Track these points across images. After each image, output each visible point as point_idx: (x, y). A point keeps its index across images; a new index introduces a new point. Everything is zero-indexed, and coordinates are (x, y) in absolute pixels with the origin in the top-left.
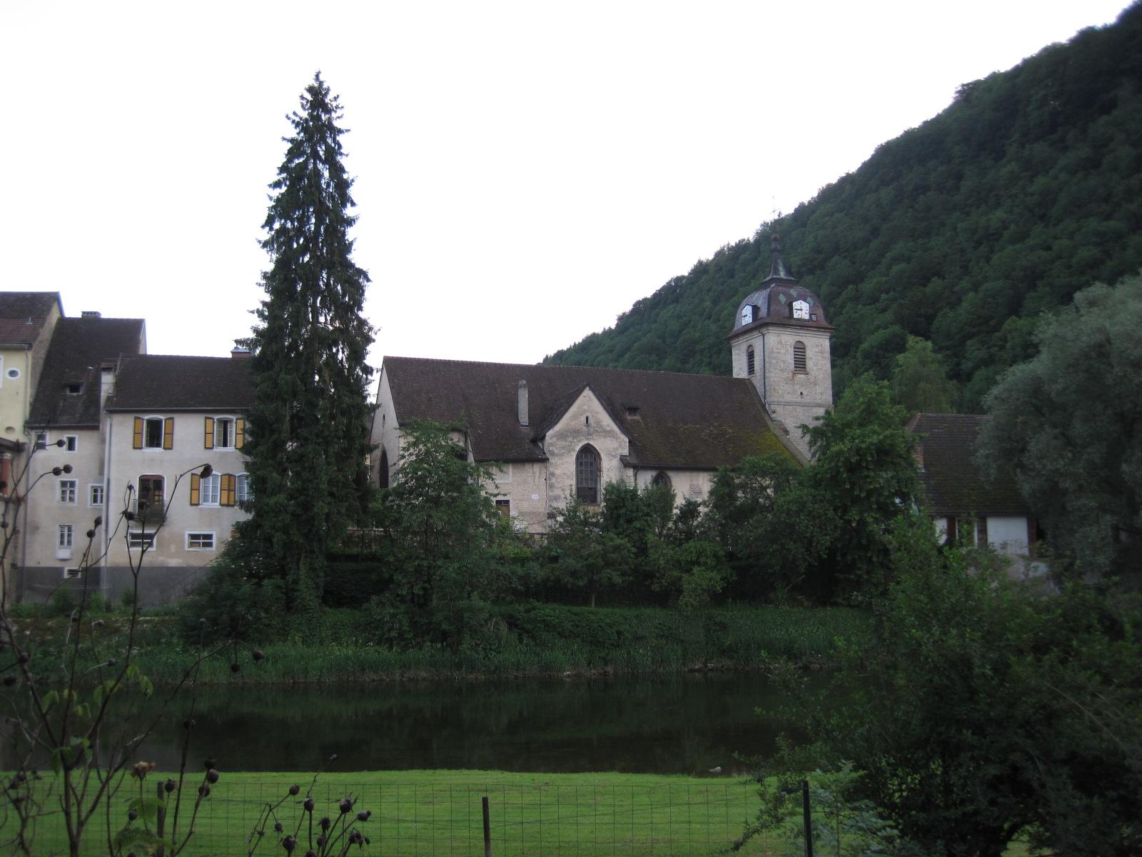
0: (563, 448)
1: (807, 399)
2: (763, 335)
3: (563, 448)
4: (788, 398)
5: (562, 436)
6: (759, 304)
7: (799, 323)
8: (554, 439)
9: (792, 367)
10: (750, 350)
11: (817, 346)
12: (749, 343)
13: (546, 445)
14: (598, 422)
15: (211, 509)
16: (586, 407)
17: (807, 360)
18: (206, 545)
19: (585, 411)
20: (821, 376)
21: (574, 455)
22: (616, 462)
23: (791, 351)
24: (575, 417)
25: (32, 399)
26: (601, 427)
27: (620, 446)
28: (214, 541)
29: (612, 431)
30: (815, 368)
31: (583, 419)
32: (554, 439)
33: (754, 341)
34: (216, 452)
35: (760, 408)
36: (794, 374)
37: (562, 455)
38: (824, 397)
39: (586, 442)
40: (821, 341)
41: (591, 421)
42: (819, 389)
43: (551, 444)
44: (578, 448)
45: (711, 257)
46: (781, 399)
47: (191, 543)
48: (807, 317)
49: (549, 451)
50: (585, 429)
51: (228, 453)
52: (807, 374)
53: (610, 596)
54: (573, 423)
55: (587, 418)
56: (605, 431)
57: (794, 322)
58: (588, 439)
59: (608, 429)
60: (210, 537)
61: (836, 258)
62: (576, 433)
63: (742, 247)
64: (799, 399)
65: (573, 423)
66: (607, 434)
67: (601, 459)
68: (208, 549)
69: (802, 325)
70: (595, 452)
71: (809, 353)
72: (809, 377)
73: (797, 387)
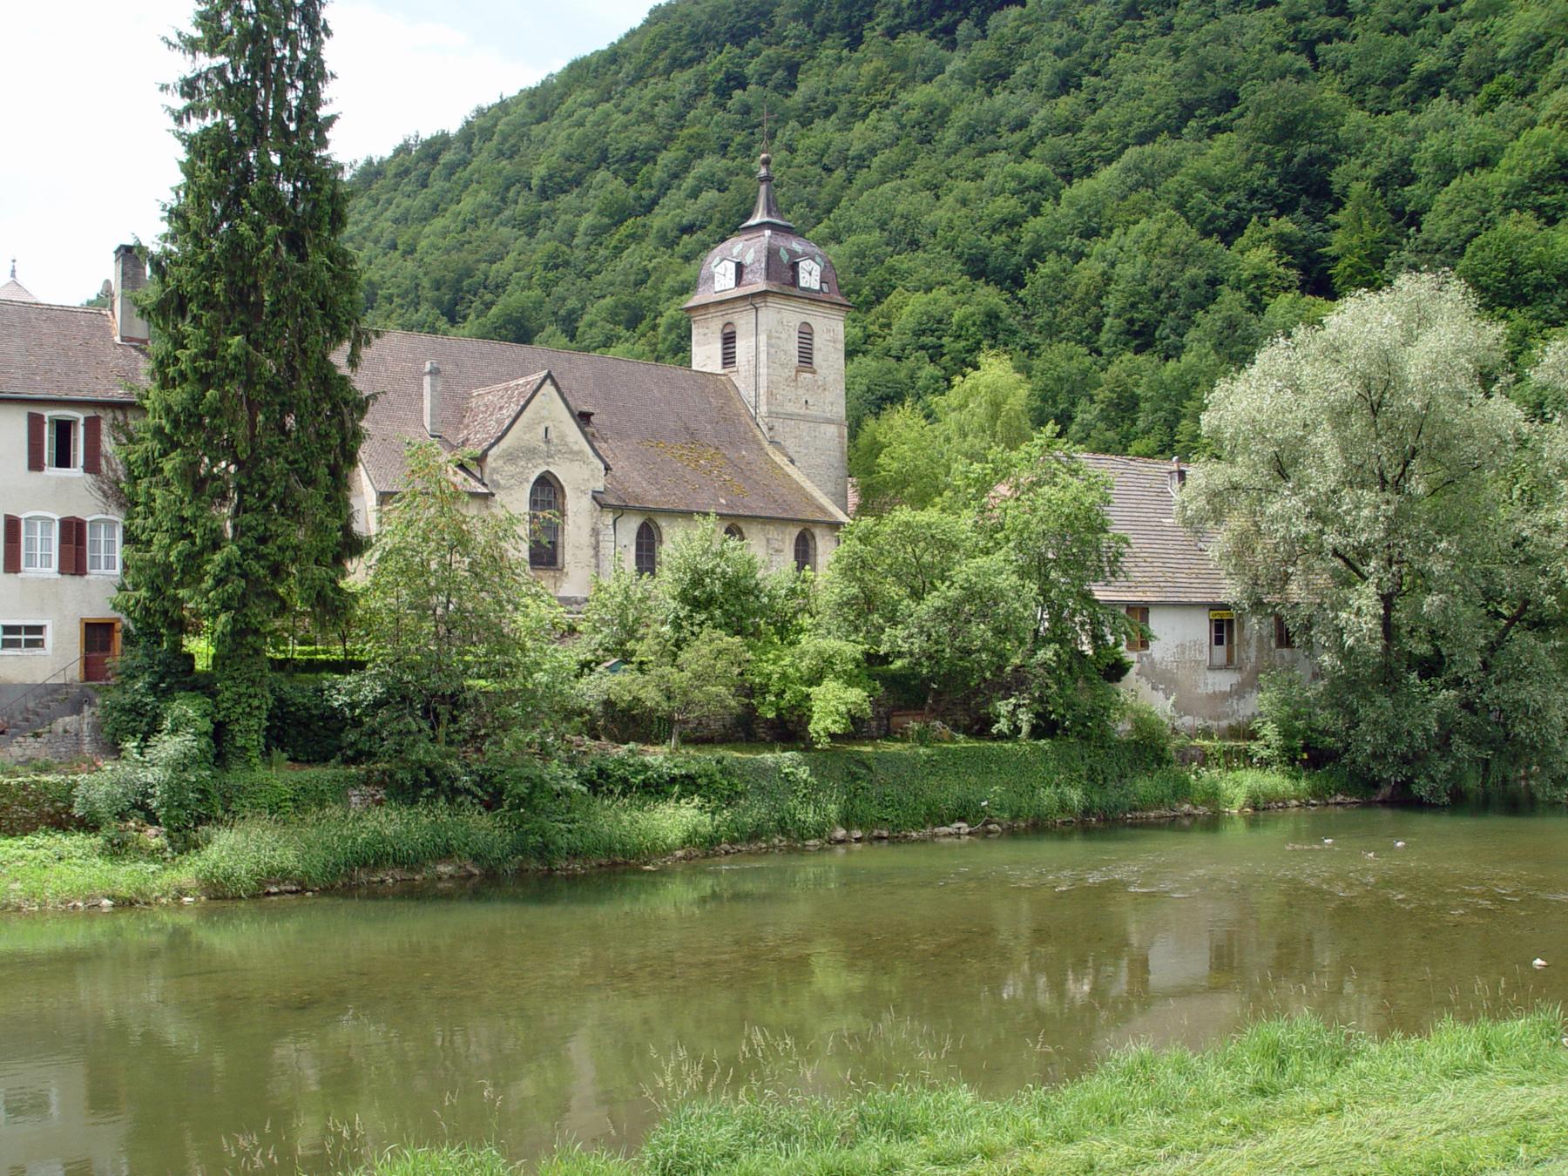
0: (513, 477)
1: (813, 411)
2: (757, 309)
3: (513, 477)
4: (790, 408)
5: (511, 457)
6: (748, 260)
7: (806, 294)
8: (500, 462)
9: (796, 360)
10: (727, 331)
11: (828, 331)
12: (728, 318)
13: (487, 471)
14: (562, 437)
15: (43, 580)
16: (544, 413)
17: (815, 352)
18: (31, 644)
19: (543, 419)
20: (832, 377)
21: (528, 487)
22: (586, 502)
23: (795, 335)
24: (530, 427)
25: (356, 478)
26: (566, 444)
27: (592, 476)
28: (48, 637)
29: (581, 452)
30: (825, 364)
31: (541, 431)
32: (500, 462)
33: (736, 316)
34: (49, 478)
35: (748, 420)
36: (797, 371)
37: (510, 488)
38: (835, 410)
39: (545, 468)
40: (833, 323)
41: (552, 435)
42: (829, 397)
43: (494, 470)
44: (533, 478)
45: (387, 153)
46: (779, 410)
47: (41, 633)
48: (817, 287)
49: (492, 481)
50: (543, 446)
51: (70, 479)
52: (814, 372)
53: (726, 739)
54: (527, 436)
55: (546, 429)
56: (572, 452)
57: (797, 292)
58: (548, 464)
59: (576, 448)
60: (39, 629)
61: (602, 174)
62: (530, 453)
63: (435, 148)
64: (802, 412)
65: (527, 436)
66: (575, 455)
67: (564, 496)
68: (37, 651)
69: (811, 297)
70: (557, 485)
71: (818, 341)
72: (817, 377)
73: (801, 392)
